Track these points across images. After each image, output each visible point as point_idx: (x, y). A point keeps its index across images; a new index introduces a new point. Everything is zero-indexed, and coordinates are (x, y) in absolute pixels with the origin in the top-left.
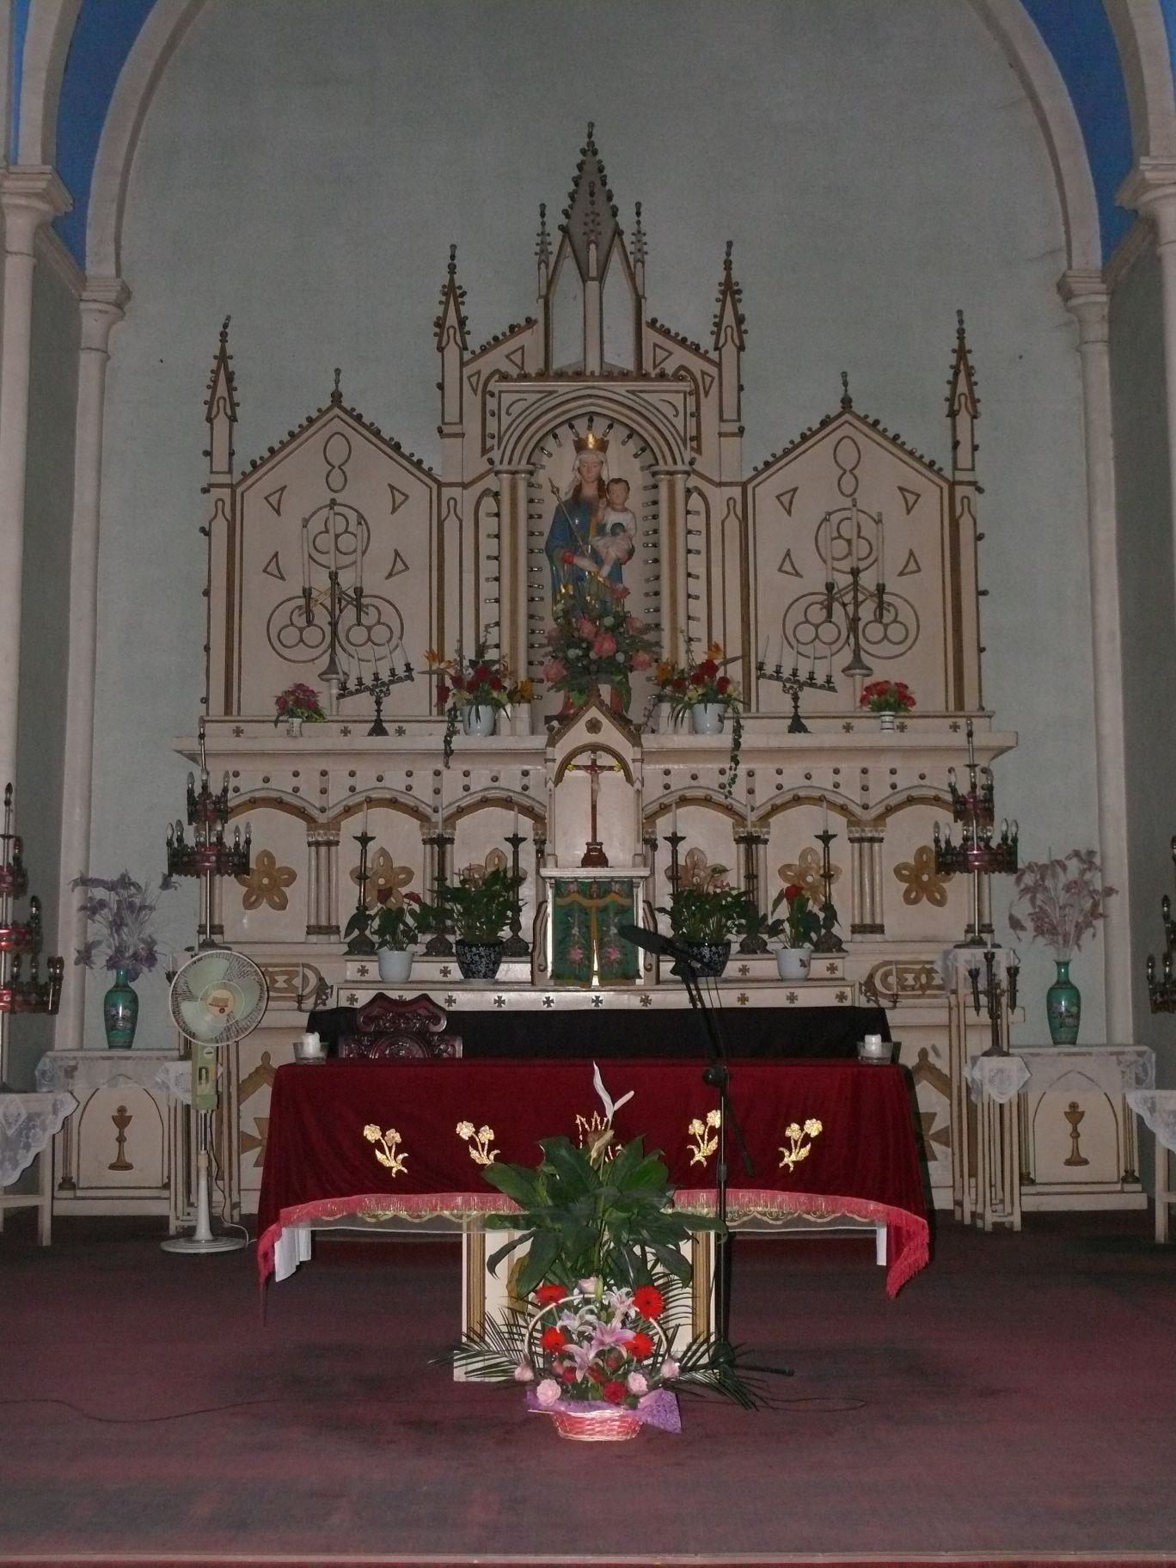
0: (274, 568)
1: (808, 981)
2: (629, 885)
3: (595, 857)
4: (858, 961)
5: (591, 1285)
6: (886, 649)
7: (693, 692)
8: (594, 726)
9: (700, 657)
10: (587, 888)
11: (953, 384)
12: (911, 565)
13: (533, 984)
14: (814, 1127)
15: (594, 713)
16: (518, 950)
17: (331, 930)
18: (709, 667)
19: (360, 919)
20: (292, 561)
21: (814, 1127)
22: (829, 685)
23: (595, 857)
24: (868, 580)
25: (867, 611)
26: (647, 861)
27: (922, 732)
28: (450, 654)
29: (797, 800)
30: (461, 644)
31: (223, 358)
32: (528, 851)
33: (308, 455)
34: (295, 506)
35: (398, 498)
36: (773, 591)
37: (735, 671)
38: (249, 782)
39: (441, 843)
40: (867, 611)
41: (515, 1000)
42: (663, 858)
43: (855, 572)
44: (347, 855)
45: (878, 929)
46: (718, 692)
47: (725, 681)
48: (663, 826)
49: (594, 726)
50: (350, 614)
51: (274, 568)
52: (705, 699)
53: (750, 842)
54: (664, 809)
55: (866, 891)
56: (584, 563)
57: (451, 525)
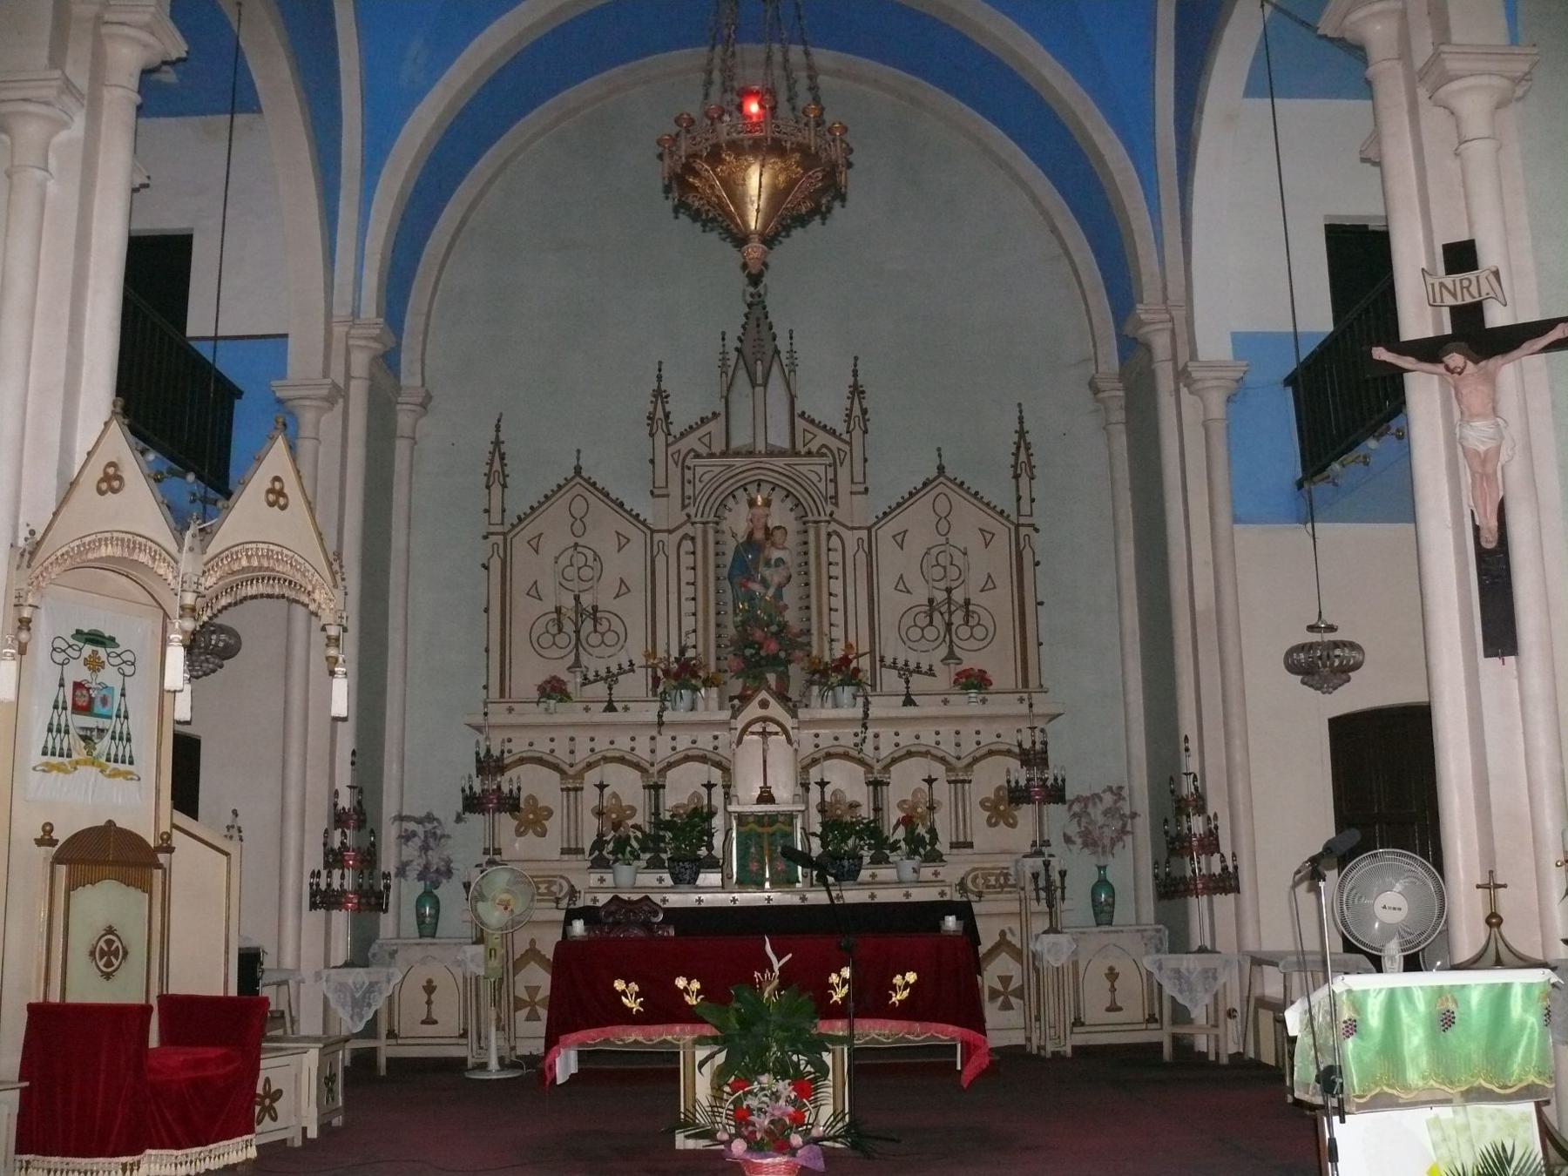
1: (919, 883)
2: (790, 817)
3: (766, 797)
4: (955, 869)
6: (975, 645)
8: (764, 704)
10: (760, 819)
11: (1016, 455)
12: (989, 584)
13: (723, 888)
14: (911, 977)
15: (764, 695)
17: (578, 851)
19: (599, 844)
20: (548, 586)
21: (911, 977)
23: (766, 797)
24: (958, 595)
25: (958, 618)
27: (998, 704)
29: (910, 754)
32: (718, 794)
34: (550, 548)
36: (892, 604)
37: (864, 663)
39: (656, 788)
40: (958, 618)
42: (815, 795)
43: (949, 590)
44: (590, 797)
48: (815, 774)
49: (764, 704)
53: (876, 785)
55: (960, 818)
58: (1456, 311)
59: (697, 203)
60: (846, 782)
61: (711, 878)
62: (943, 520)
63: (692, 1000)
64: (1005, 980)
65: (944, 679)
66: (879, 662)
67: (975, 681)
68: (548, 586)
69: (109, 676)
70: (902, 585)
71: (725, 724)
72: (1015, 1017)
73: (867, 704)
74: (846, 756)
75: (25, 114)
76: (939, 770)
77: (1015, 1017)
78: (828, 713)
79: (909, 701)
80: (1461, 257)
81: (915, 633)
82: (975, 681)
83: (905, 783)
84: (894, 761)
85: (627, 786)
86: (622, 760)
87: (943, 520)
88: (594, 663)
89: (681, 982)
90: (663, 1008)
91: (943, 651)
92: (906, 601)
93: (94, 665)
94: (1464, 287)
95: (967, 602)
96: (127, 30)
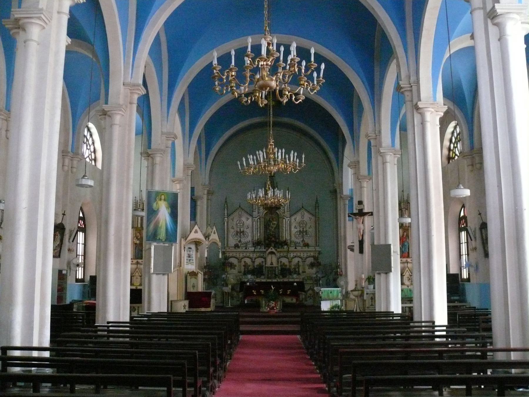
0: (233, 228)
1: (297, 278)
2: (275, 267)
3: (272, 264)
4: (303, 276)
5: (272, 302)
6: (307, 238)
7: (283, 244)
8: (271, 249)
9: (284, 240)
10: (271, 267)
11: (316, 204)
12: (310, 227)
13: (264, 279)
14: (290, 291)
15: (272, 247)
16: (263, 275)
17: (241, 272)
18: (285, 241)
19: (245, 271)
20: (235, 227)
21: (290, 291)
22: (299, 243)
23: (272, 264)
24: (305, 230)
25: (304, 234)
26: (278, 265)
27: (311, 249)
28: (254, 239)
29: (295, 257)
30: (256, 238)
31: (226, 202)
32: (264, 264)
33: (236, 214)
34: (235, 220)
35: (248, 219)
36: (294, 230)
37: (289, 241)
38: (231, 255)
39: (254, 262)
40: (304, 234)
41: (263, 281)
42: (279, 264)
43: (303, 229)
44: (243, 263)
45: (305, 272)
46: (286, 244)
47: (287, 243)
48: (280, 260)
49: (271, 249)
50: (242, 234)
51: (233, 228)
52: (285, 245)
53: (290, 262)
54: (280, 258)
55: (304, 268)
56: (270, 228)
57: (254, 223)
58: (359, 210)
59: (249, 53)
60: (285, 261)
61: (263, 277)
62: (303, 216)
63: (262, 293)
64: (310, 294)
65: (302, 244)
66: (291, 242)
67: (307, 245)
68: (235, 227)
69: (191, 253)
70: (295, 227)
71: (265, 252)
72: (311, 300)
73: (289, 248)
74: (285, 257)
75: (116, 113)
76: (300, 260)
77: (311, 300)
78: (282, 250)
79: (296, 248)
80: (360, 203)
81: (297, 236)
82: (307, 245)
83: (296, 260)
84: (293, 258)
85: (248, 261)
86: (248, 257)
87: (303, 216)
88: (243, 240)
89: (261, 291)
90: (259, 294)
91: (302, 239)
92: (296, 230)
93: (190, 251)
94: (360, 207)
95: (306, 231)
96: (170, 139)
